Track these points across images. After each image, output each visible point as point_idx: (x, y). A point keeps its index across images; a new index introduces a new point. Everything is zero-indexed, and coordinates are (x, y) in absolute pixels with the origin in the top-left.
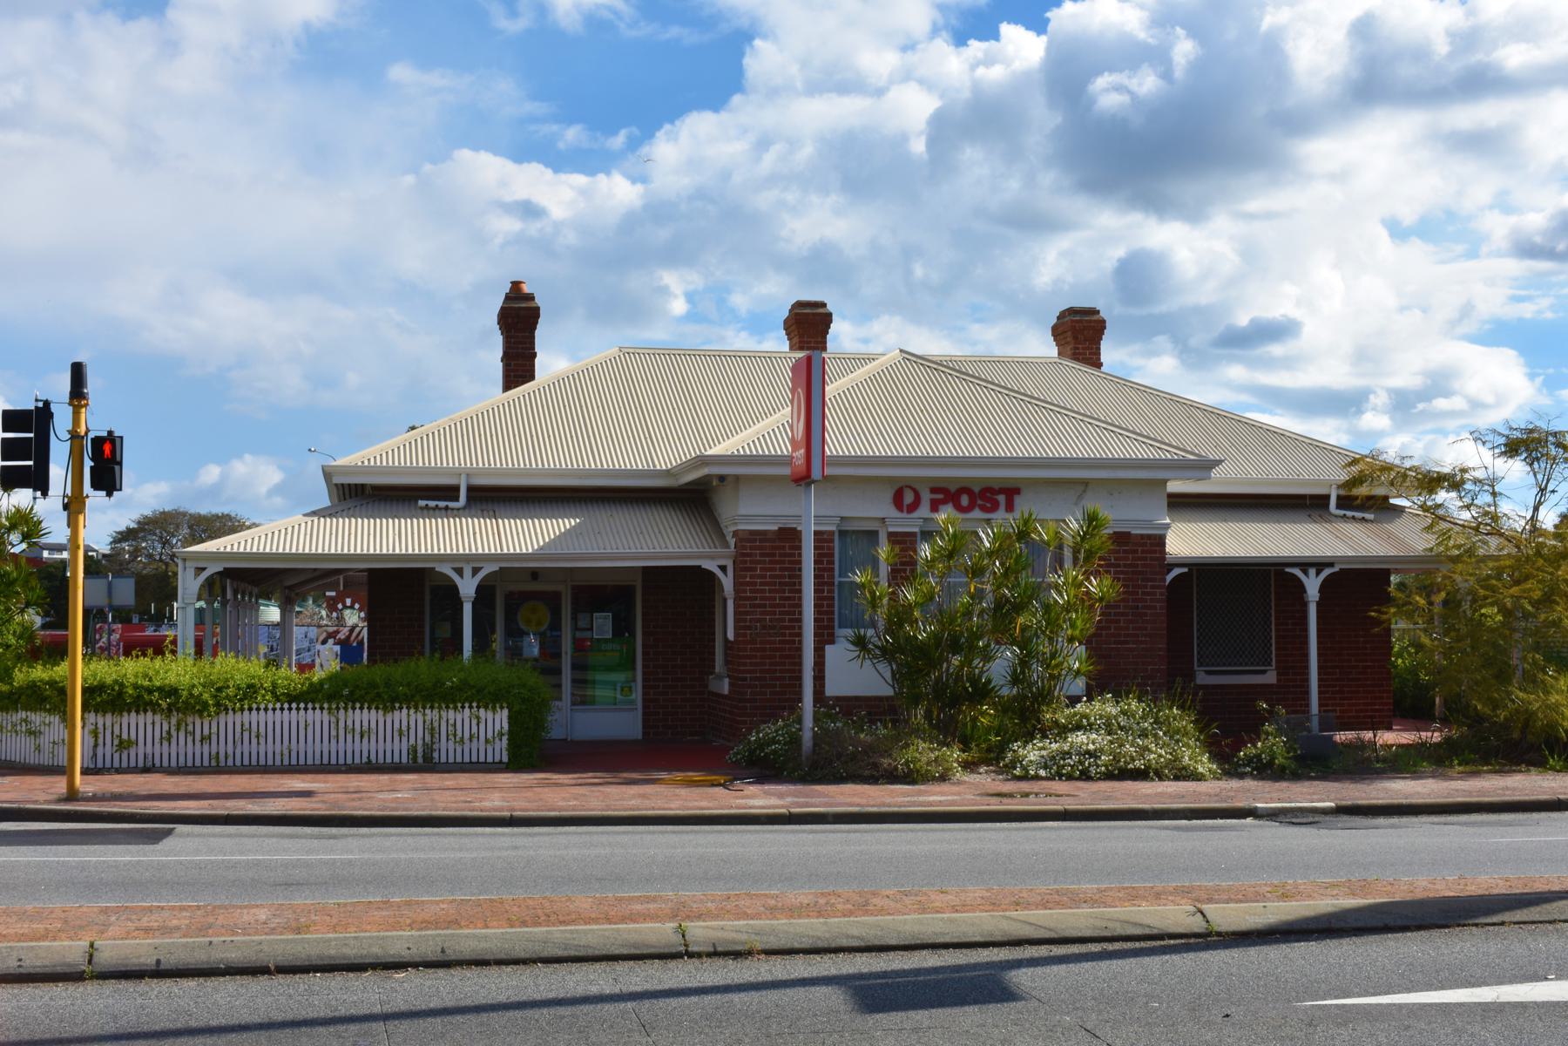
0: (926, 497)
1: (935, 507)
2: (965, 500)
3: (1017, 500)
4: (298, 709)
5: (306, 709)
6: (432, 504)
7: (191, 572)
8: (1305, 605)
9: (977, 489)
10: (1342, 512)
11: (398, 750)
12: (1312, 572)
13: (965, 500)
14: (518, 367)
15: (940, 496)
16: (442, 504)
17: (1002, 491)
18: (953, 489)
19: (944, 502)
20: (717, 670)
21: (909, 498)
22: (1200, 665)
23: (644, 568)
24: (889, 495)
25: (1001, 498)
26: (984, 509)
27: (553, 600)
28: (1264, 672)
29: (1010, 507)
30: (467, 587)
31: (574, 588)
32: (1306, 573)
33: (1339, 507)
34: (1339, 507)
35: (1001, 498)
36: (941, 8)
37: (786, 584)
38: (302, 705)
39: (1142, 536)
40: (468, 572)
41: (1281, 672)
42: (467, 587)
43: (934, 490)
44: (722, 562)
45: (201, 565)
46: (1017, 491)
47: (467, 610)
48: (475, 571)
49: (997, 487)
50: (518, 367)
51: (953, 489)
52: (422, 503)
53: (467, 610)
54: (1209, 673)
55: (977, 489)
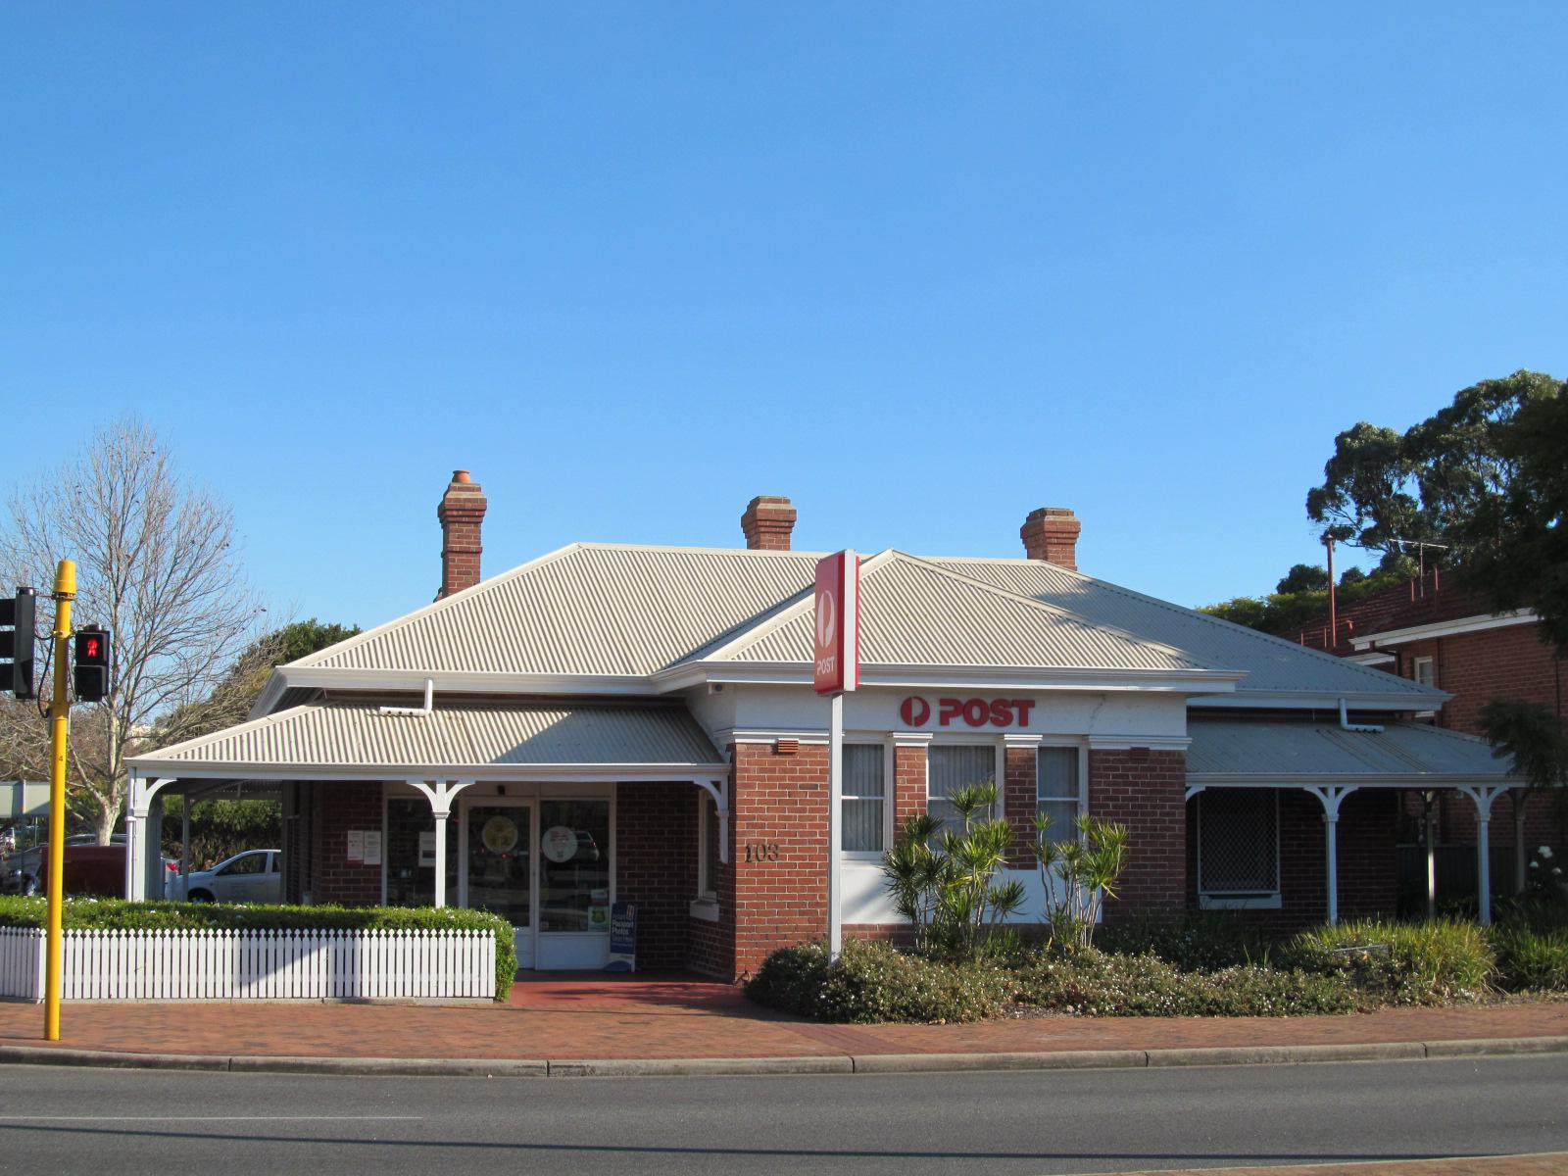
0: (935, 709)
1: (944, 719)
2: (976, 713)
3: (1033, 713)
4: (163, 936)
5: (276, 936)
6: (395, 710)
7: (142, 782)
8: (1324, 825)
9: (989, 701)
10: (1354, 727)
11: (111, 993)
12: (441, 787)
13: (976, 713)
14: (459, 566)
15: (950, 708)
16: (406, 711)
17: (1014, 704)
18: (964, 700)
19: (955, 714)
20: (700, 893)
21: (917, 710)
22: (1204, 888)
23: (619, 783)
24: (894, 707)
25: (1015, 711)
26: (997, 723)
27: (520, 816)
28: (1268, 896)
29: (1024, 722)
30: (441, 801)
31: (544, 803)
32: (433, 785)
33: (1350, 721)
34: (1350, 721)
35: (1015, 711)
36: (1564, 388)
37: (786, 802)
38: (150, 932)
39: (1161, 752)
40: (1331, 792)
41: (1287, 895)
42: (441, 801)
43: (943, 702)
44: (715, 778)
45: (152, 775)
46: (1032, 704)
47: (441, 826)
48: (1338, 791)
49: (1010, 698)
50: (459, 566)
51: (964, 700)
52: (384, 709)
53: (441, 826)
54: (1212, 897)
55: (989, 701)
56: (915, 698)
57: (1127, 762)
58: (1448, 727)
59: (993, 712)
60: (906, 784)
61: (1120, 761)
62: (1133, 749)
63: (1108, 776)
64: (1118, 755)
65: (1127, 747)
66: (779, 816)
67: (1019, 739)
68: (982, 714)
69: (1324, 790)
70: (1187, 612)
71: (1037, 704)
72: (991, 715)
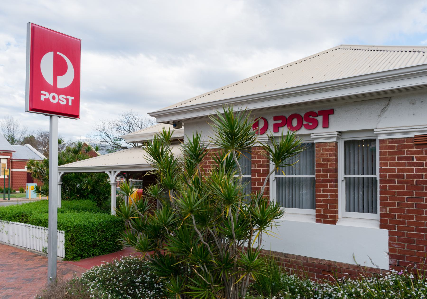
0: (272, 123)
1: (276, 128)
13: (295, 123)
15: (280, 122)
26: (308, 127)
29: (326, 125)
35: (320, 119)
40: (113, 173)
46: (332, 112)
56: (262, 118)
57: (411, 147)
58: (47, 220)
59: (306, 121)
60: (256, 168)
61: (404, 147)
62: (416, 136)
63: (394, 159)
64: (403, 142)
65: (412, 136)
66: (387, 166)
67: (320, 134)
68: (293, 119)
69: (111, 172)
70: (301, 262)
71: (335, 112)
72: (305, 123)
